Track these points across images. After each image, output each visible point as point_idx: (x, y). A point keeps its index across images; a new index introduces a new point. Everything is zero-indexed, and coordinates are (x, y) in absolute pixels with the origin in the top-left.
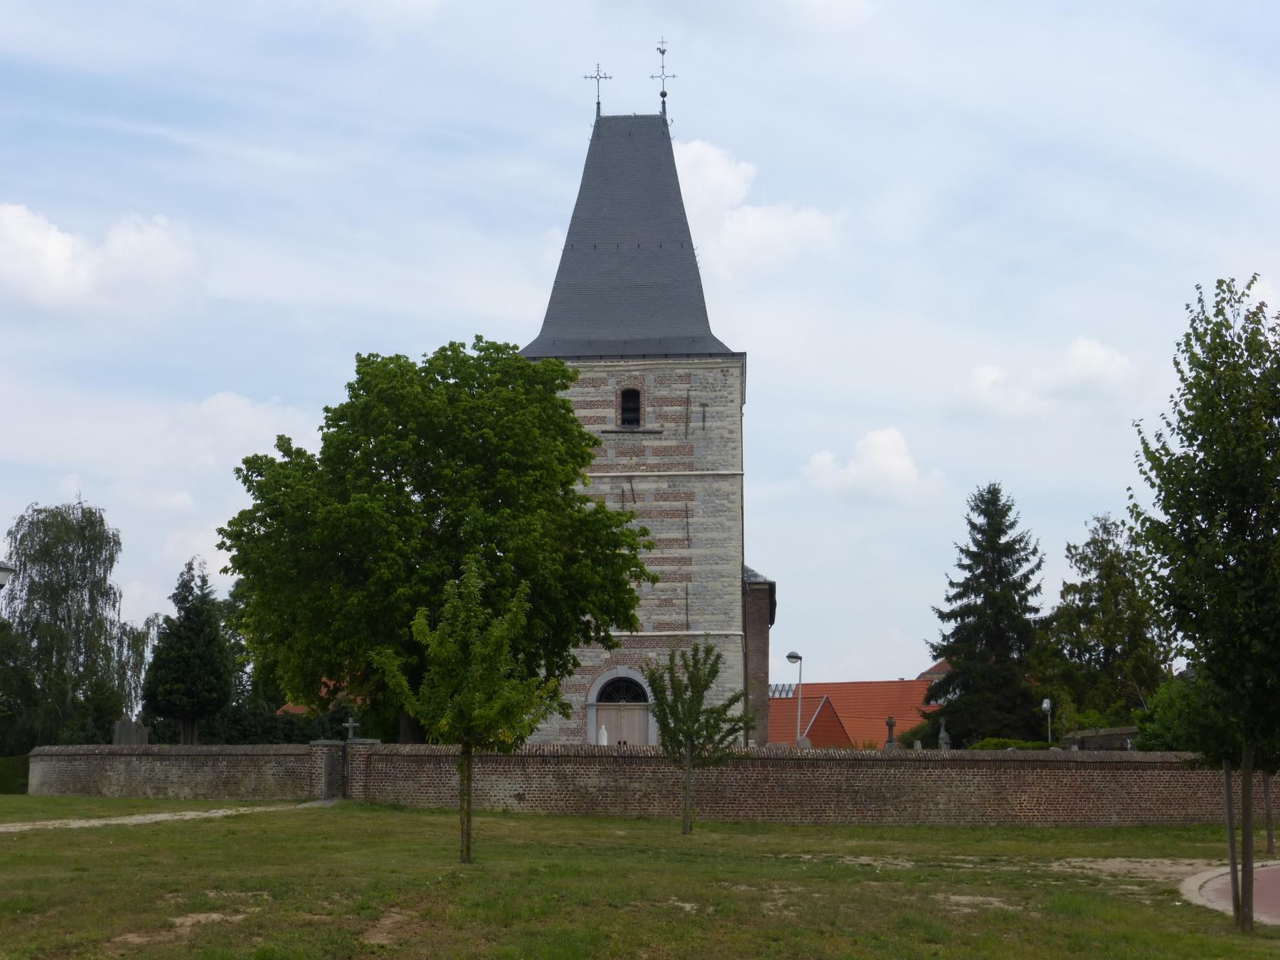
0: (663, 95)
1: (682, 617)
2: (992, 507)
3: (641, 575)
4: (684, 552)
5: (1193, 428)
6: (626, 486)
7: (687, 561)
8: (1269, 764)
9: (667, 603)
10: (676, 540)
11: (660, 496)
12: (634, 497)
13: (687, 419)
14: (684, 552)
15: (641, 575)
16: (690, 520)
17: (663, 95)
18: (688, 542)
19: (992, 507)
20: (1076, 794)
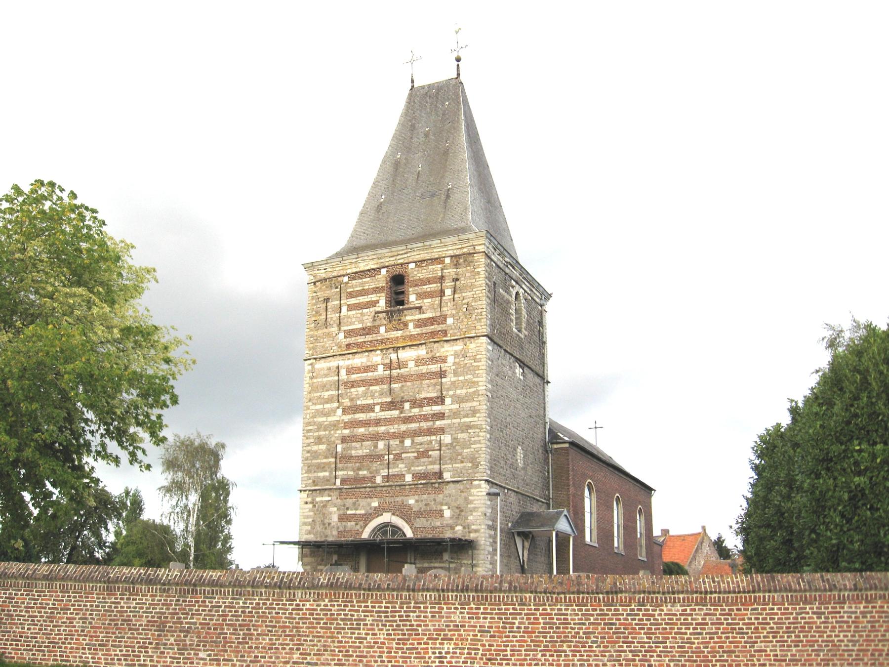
0: (458, 60)
1: (436, 468)
2: (437, 120)
3: (747, 499)
4: (437, 408)
5: (807, 400)
6: (394, 356)
7: (441, 416)
8: (886, 570)
9: (424, 454)
10: (431, 399)
11: (419, 362)
12: (401, 365)
13: (442, 293)
14: (437, 408)
15: (747, 499)
16: (444, 380)
17: (458, 60)
18: (441, 400)
19: (437, 120)
20: (537, 643)
